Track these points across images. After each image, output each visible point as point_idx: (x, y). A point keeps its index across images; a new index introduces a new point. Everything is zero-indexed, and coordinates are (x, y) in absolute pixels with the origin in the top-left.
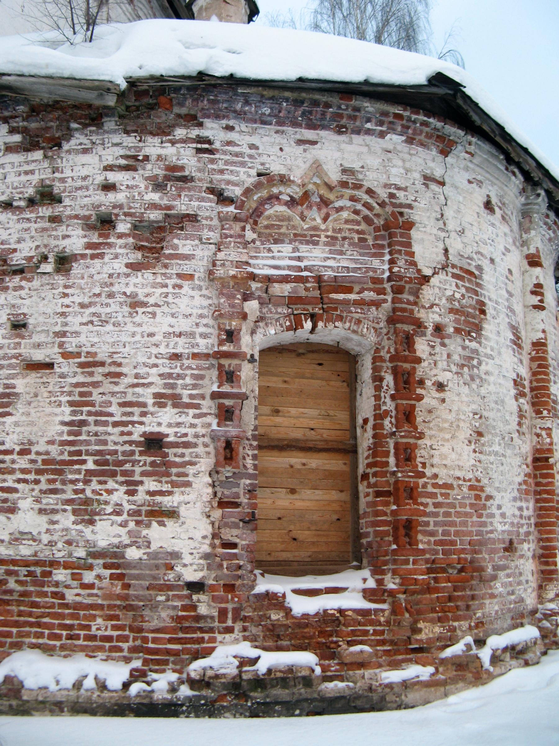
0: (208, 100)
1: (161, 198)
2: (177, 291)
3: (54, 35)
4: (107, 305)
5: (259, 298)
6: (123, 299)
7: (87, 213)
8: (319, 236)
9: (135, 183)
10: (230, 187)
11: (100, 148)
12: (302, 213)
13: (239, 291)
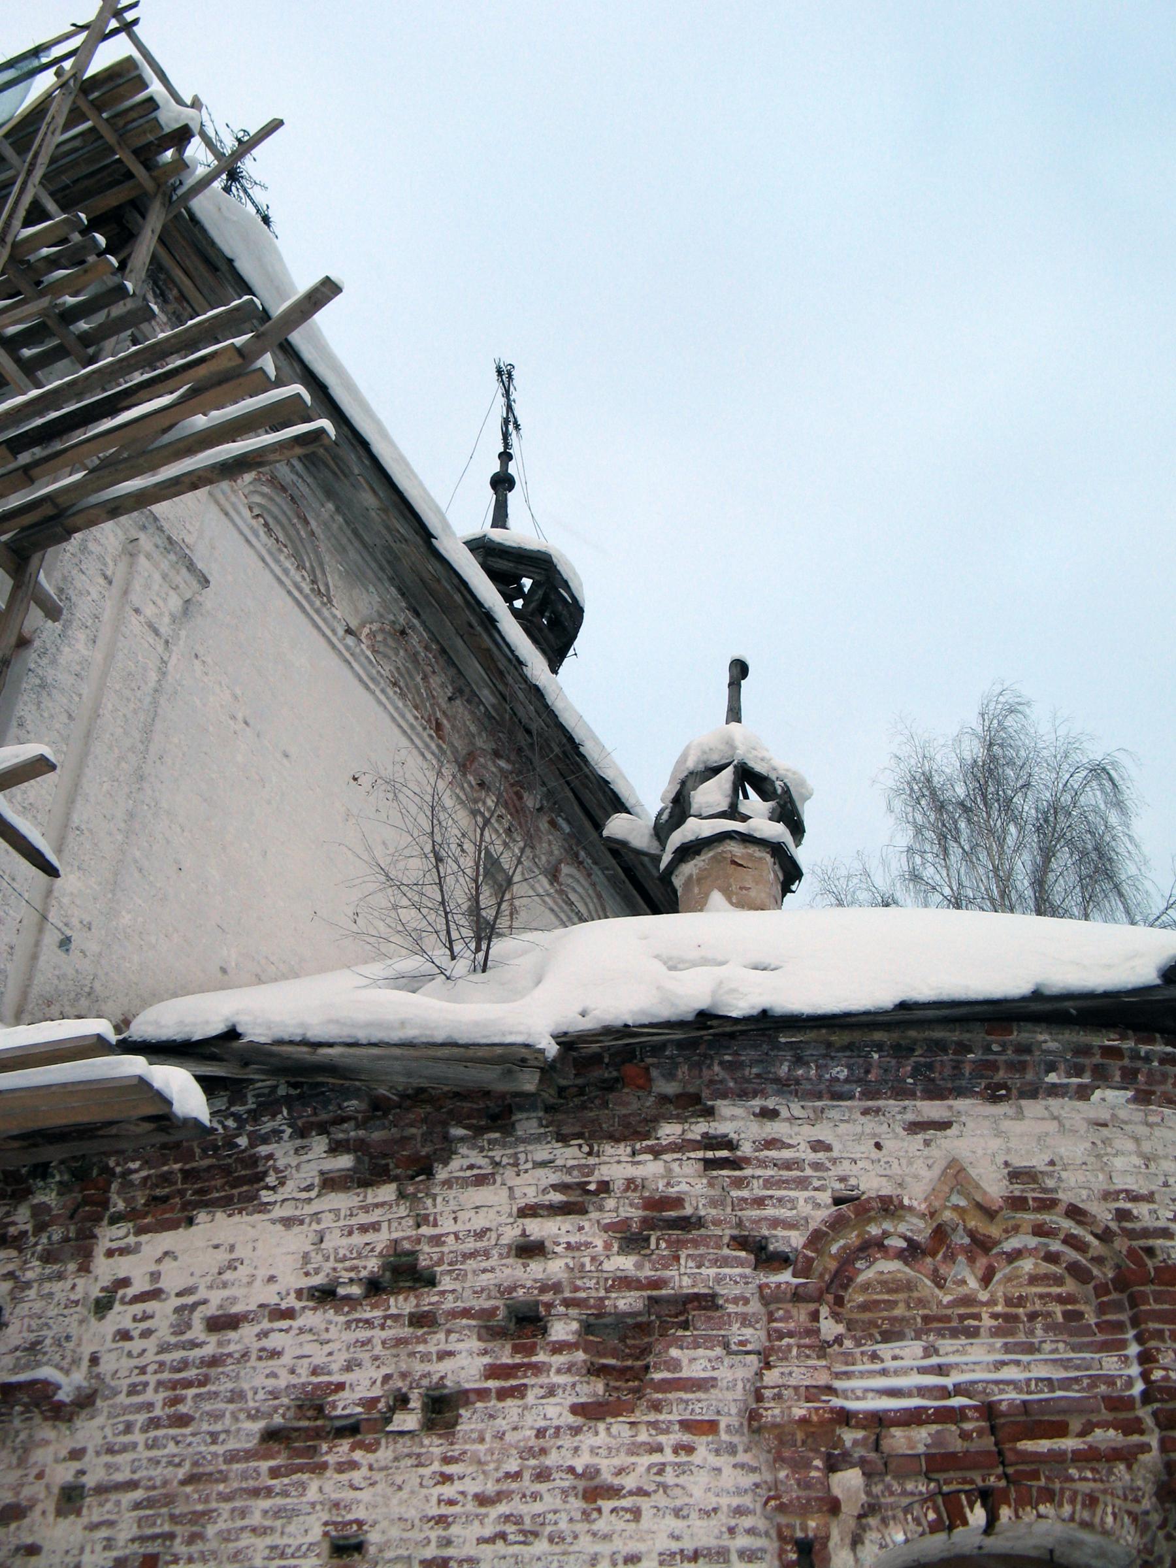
0: (721, 1063)
1: (639, 1266)
2: (683, 1458)
3: (413, 964)
4: (536, 1496)
5: (862, 1463)
6: (567, 1482)
7: (488, 1304)
8: (977, 1317)
9: (583, 1239)
10: (780, 1232)
11: (510, 1173)
12: (936, 1270)
13: (817, 1451)
